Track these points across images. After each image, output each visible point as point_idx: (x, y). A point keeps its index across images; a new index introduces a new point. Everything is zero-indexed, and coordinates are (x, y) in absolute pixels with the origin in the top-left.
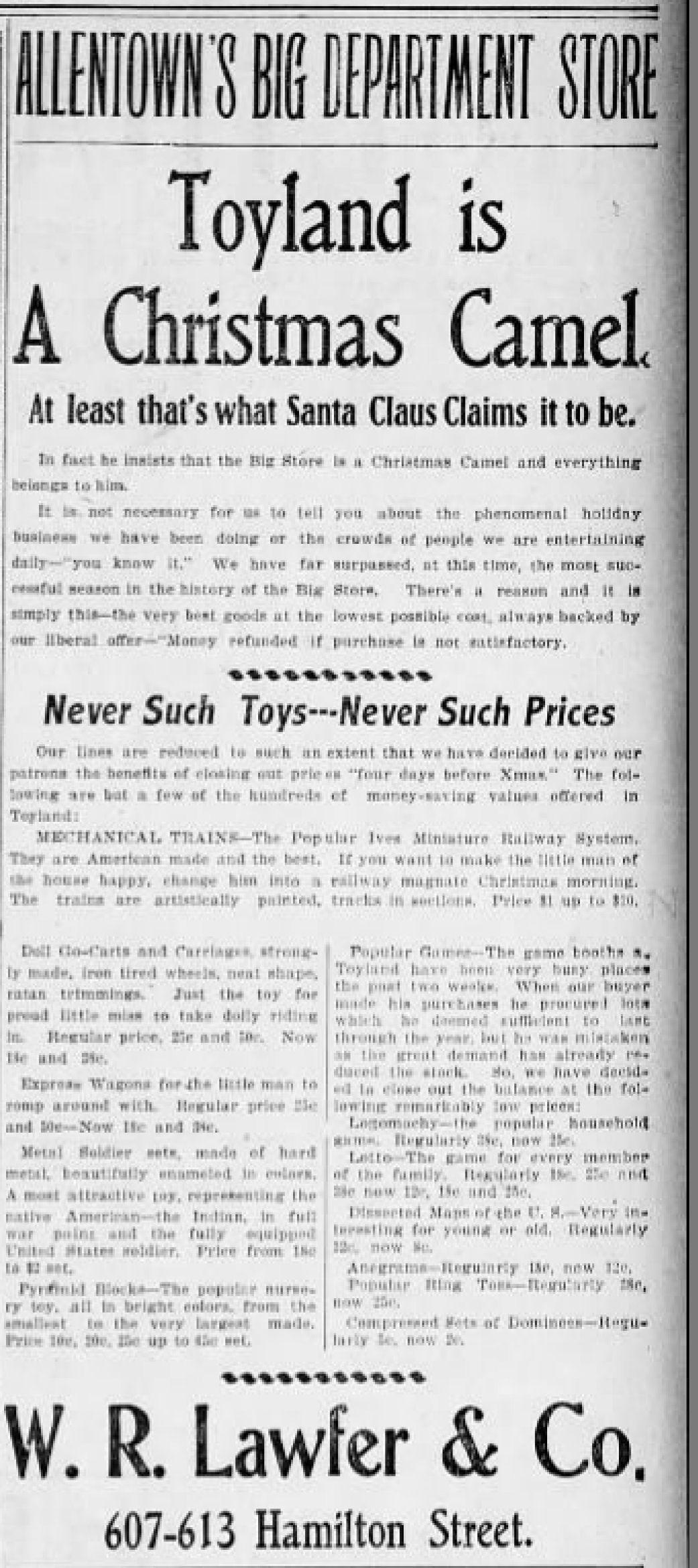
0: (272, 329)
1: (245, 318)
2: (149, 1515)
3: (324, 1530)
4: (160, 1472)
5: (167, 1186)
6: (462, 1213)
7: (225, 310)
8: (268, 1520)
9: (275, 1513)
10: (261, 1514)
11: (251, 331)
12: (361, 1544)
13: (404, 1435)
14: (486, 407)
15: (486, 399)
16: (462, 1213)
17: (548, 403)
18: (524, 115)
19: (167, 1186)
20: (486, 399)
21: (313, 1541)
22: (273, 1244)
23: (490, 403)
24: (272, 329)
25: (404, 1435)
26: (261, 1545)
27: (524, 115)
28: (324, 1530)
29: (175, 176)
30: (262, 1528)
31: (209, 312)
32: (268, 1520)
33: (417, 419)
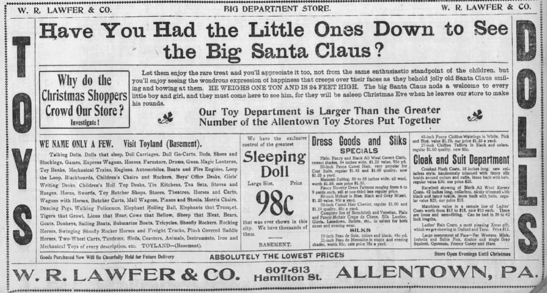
0: (67, 95)
1: (62, 94)
5: (169, 212)
6: (427, 110)
7: (59, 92)
11: (63, 96)
13: (440, 119)
14: (285, 155)
15: (285, 152)
16: (427, 110)
17: (270, 25)
19: (169, 212)
20: (285, 152)
22: (319, 224)
23: (287, 154)
24: (67, 95)
25: (440, 119)
29: (222, 109)
31: (57, 93)
33: (354, 143)
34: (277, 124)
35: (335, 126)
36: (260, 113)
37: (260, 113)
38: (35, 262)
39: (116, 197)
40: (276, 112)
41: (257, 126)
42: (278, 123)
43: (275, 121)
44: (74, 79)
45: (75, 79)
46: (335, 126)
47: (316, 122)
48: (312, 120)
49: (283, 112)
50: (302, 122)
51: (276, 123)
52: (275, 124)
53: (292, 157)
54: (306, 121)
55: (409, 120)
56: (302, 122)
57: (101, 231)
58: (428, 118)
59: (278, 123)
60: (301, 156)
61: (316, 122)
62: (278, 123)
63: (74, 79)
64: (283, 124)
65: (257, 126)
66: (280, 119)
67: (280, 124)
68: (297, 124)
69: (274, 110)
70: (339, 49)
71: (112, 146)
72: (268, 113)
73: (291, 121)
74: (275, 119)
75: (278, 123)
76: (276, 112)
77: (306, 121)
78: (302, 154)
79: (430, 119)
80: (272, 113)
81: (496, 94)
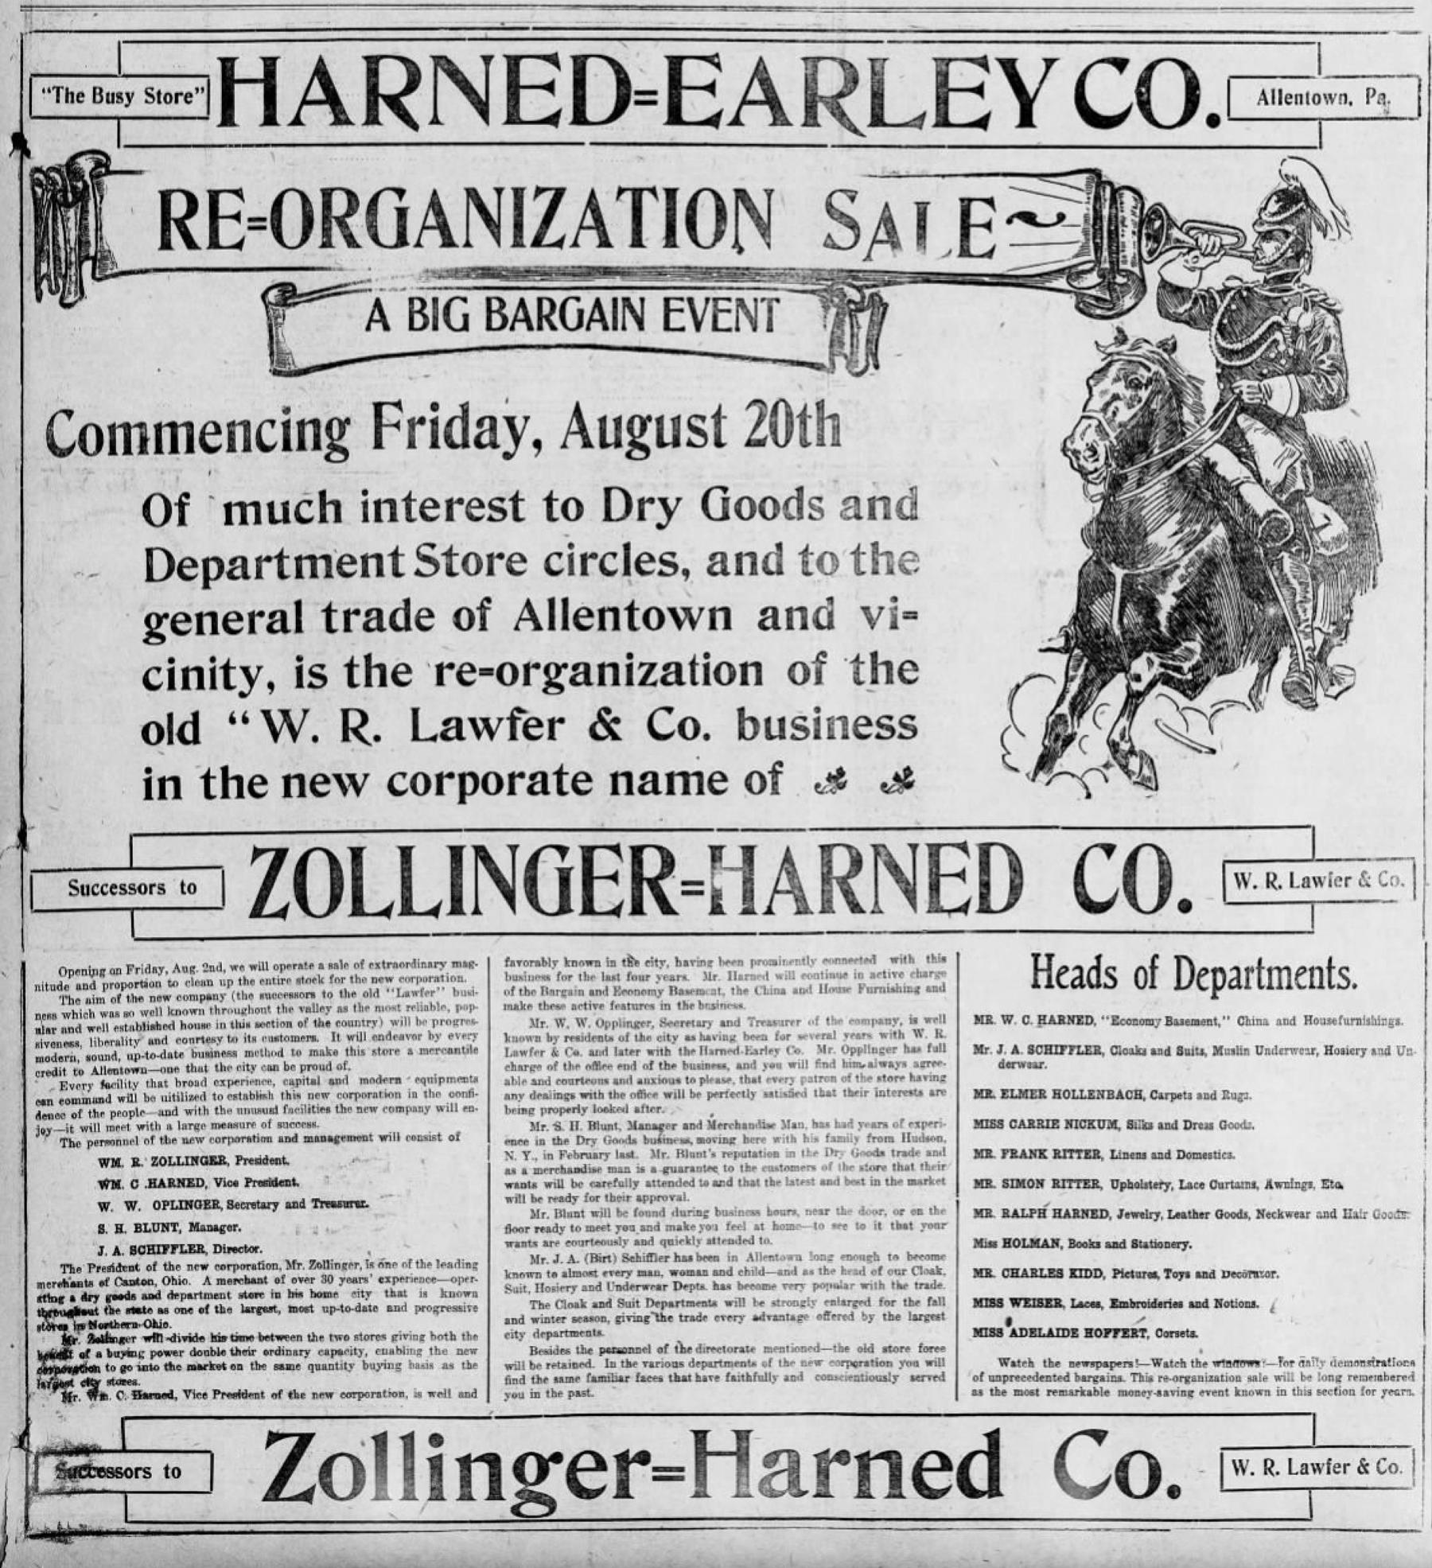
2: (761, 443)
3: (1285, 973)
4: (517, 628)
8: (1043, 963)
9: (1050, 956)
10: (1036, 956)
12: (561, 792)
18: (770, 329)
21: (1275, 984)
26: (1036, 985)
27: (770, 329)
28: (1285, 973)
30: (1036, 969)
32: (1043, 963)
34: (538, 627)
35: (507, 456)
36: (213, 568)
37: (213, 568)
38: (1310, 856)
39: (551, 1000)
40: (290, 567)
41: (340, 633)
42: (544, 621)
43: (531, 611)
44: (510, 421)
45: (519, 423)
46: (507, 456)
47: (720, 617)
48: (701, 609)
49: (321, 565)
50: (654, 619)
51: (534, 618)
52: (530, 625)
53: (480, 1472)
54: (673, 611)
55: (426, 778)
56: (654, 619)
57: (1164, 1021)
58: (375, 661)
59: (544, 620)
60: (531, 1469)
61: (720, 617)
62: (544, 620)
63: (510, 421)
64: (565, 627)
65: (340, 633)
66: (552, 602)
67: (552, 627)
68: (632, 627)
69: (281, 557)
70: (480, 423)
71: (707, 737)
72: (252, 570)
73: (602, 612)
74: (528, 604)
75: (544, 621)
76: (290, 567)
77: (673, 611)
78: (538, 1457)
79: (382, 667)
80: (269, 570)
81: (250, 1338)
